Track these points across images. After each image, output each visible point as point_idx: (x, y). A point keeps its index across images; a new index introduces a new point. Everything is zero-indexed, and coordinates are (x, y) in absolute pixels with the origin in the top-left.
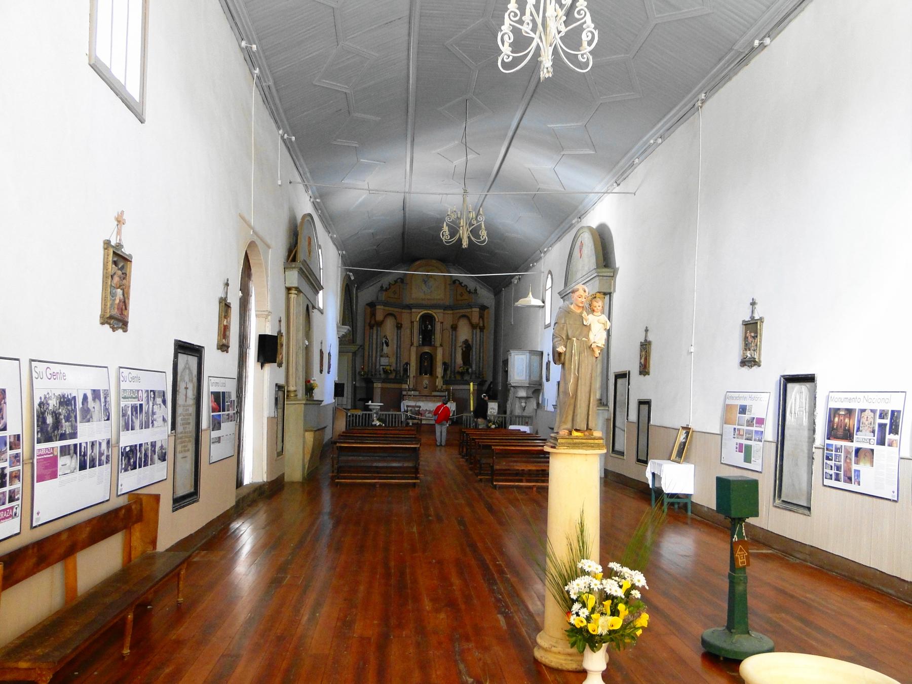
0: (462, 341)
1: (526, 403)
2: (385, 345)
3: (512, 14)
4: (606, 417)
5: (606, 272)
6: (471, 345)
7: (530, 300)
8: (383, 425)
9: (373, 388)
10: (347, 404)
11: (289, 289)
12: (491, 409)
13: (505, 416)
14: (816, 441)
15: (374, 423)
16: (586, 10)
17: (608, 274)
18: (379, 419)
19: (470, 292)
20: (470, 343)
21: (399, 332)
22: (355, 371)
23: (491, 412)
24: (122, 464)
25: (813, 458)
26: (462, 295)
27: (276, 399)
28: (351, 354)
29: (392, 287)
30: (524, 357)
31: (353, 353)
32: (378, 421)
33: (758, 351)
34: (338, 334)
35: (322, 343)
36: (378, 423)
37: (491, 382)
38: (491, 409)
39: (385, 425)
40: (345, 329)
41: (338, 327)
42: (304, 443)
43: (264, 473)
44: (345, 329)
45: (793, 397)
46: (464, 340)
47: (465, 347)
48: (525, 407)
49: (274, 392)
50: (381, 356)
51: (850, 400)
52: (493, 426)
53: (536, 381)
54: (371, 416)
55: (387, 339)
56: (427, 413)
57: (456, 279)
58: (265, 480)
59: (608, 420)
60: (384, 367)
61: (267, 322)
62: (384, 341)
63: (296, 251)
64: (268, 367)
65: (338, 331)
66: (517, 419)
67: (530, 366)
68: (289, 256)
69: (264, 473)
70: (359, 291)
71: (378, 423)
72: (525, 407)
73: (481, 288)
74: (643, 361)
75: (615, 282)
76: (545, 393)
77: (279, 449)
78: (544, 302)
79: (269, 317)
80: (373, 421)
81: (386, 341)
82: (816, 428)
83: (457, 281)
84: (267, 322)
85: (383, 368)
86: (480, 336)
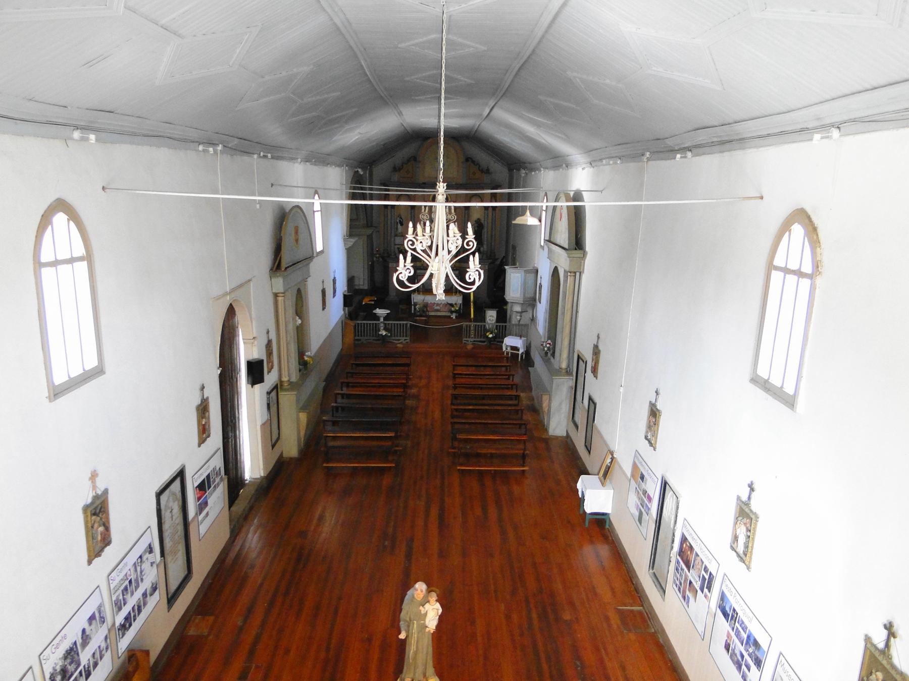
0: (474, 220)
1: (521, 316)
2: (399, 225)
3: (410, 243)
4: (571, 385)
5: (578, 253)
6: (483, 224)
7: (527, 220)
8: (389, 334)
9: (388, 267)
10: (363, 285)
11: (276, 295)
12: (491, 316)
13: (506, 324)
14: (674, 548)
15: (380, 333)
16: (474, 241)
17: (578, 255)
18: (385, 329)
19: (482, 171)
20: (482, 222)
21: (413, 211)
22: (372, 249)
23: (490, 320)
24: (119, 635)
25: (670, 561)
26: (474, 173)
27: (268, 405)
28: (366, 236)
29: (405, 166)
30: (519, 275)
31: (368, 236)
32: (384, 331)
33: (655, 436)
34: (345, 246)
35: (323, 282)
36: (384, 333)
37: (504, 257)
38: (491, 316)
39: (391, 334)
40: (352, 242)
41: (345, 240)
42: (298, 424)
43: (261, 470)
44: (352, 242)
45: (669, 497)
46: (476, 219)
47: (478, 227)
48: (520, 320)
49: (266, 399)
50: (396, 235)
51: (691, 534)
52: (491, 336)
53: (530, 298)
54: (378, 326)
55: (402, 219)
56: (435, 305)
57: (469, 156)
58: (262, 475)
59: (572, 387)
60: (399, 246)
61: (254, 347)
62: (398, 221)
63: (280, 258)
64: (257, 386)
65: (345, 244)
66: (515, 327)
67: (525, 284)
68: (274, 263)
69: (261, 470)
70: (373, 166)
71: (384, 333)
72: (520, 320)
73: (495, 162)
74: (593, 363)
75: (584, 263)
76: (538, 309)
77: (275, 437)
78: (540, 221)
79: (256, 343)
80: (379, 331)
81: (400, 221)
82: (675, 539)
83: (469, 159)
84: (254, 347)
85: (398, 248)
86: (493, 215)
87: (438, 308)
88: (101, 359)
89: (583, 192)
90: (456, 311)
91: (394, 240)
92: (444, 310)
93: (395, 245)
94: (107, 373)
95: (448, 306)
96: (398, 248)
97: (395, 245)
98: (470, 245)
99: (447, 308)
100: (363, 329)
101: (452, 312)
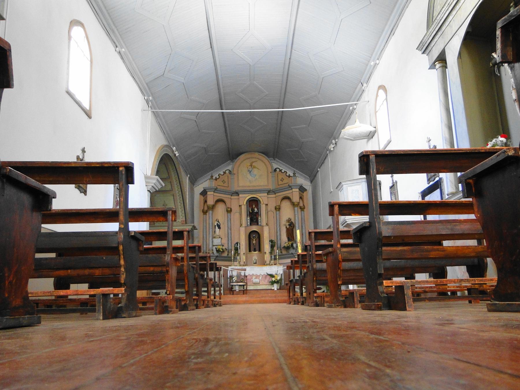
20: (293, 220)
26: (282, 180)
55: (219, 222)
56: (254, 277)
81: (217, 224)
87: (257, 280)
88: (87, 35)
89: (438, 190)
90: (277, 282)
91: (213, 242)
92: (264, 283)
93: (213, 246)
94: (92, 119)
95: (269, 277)
96: (216, 248)
97: (213, 246)
98: (292, 226)
99: (266, 281)
100: (229, 236)
101: (273, 283)
